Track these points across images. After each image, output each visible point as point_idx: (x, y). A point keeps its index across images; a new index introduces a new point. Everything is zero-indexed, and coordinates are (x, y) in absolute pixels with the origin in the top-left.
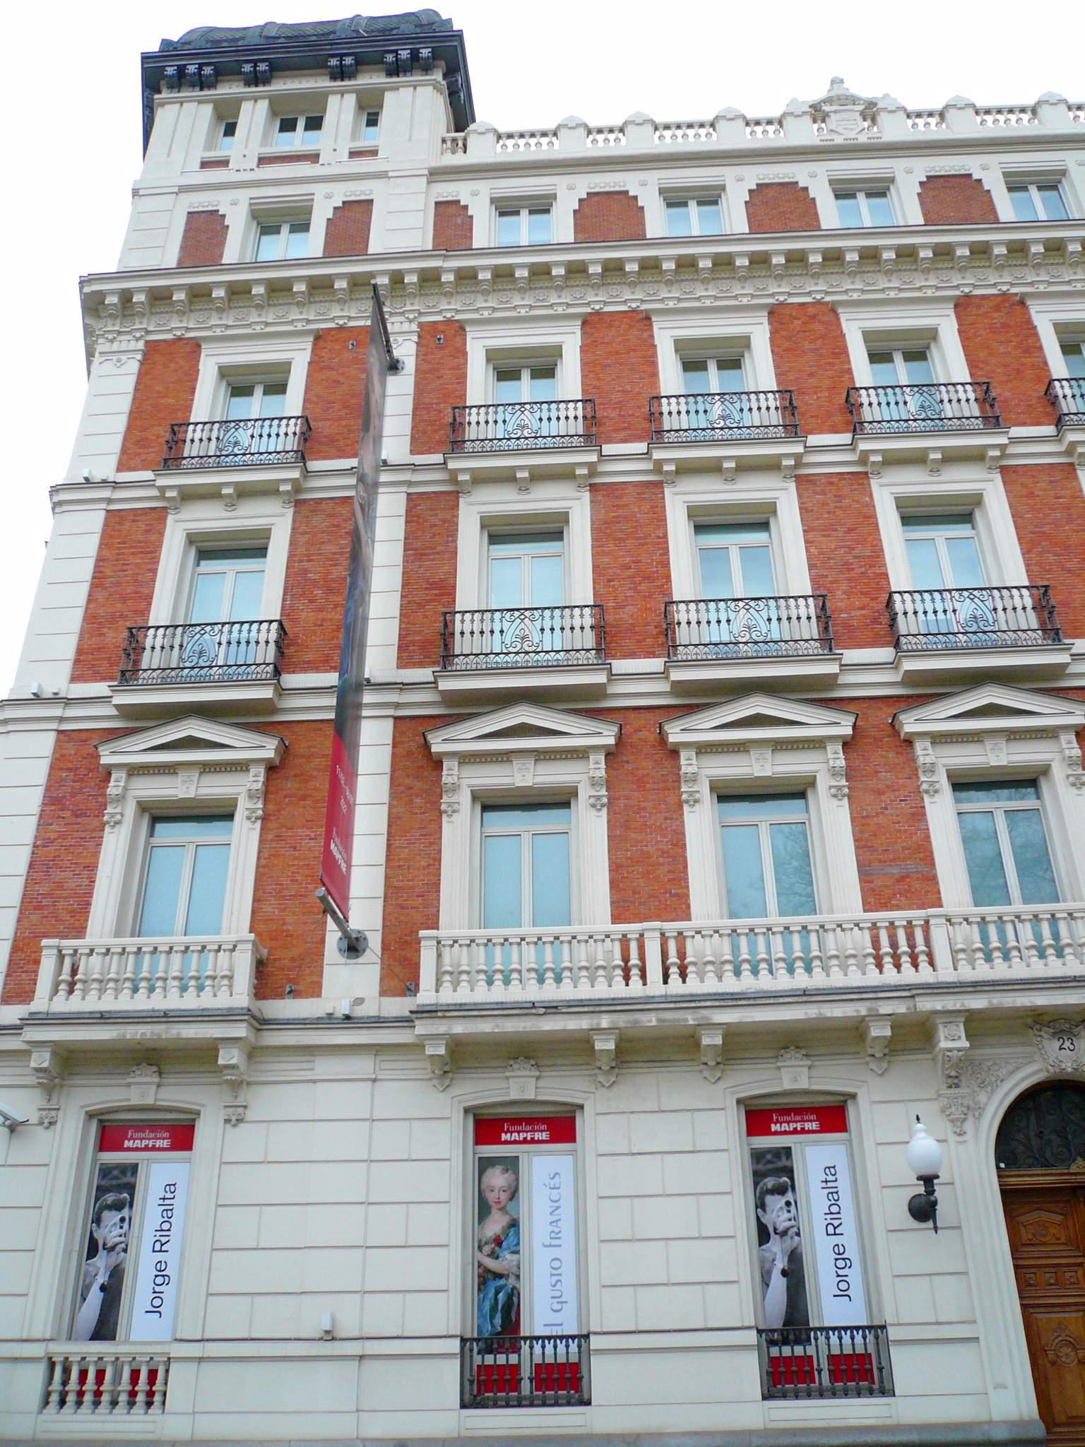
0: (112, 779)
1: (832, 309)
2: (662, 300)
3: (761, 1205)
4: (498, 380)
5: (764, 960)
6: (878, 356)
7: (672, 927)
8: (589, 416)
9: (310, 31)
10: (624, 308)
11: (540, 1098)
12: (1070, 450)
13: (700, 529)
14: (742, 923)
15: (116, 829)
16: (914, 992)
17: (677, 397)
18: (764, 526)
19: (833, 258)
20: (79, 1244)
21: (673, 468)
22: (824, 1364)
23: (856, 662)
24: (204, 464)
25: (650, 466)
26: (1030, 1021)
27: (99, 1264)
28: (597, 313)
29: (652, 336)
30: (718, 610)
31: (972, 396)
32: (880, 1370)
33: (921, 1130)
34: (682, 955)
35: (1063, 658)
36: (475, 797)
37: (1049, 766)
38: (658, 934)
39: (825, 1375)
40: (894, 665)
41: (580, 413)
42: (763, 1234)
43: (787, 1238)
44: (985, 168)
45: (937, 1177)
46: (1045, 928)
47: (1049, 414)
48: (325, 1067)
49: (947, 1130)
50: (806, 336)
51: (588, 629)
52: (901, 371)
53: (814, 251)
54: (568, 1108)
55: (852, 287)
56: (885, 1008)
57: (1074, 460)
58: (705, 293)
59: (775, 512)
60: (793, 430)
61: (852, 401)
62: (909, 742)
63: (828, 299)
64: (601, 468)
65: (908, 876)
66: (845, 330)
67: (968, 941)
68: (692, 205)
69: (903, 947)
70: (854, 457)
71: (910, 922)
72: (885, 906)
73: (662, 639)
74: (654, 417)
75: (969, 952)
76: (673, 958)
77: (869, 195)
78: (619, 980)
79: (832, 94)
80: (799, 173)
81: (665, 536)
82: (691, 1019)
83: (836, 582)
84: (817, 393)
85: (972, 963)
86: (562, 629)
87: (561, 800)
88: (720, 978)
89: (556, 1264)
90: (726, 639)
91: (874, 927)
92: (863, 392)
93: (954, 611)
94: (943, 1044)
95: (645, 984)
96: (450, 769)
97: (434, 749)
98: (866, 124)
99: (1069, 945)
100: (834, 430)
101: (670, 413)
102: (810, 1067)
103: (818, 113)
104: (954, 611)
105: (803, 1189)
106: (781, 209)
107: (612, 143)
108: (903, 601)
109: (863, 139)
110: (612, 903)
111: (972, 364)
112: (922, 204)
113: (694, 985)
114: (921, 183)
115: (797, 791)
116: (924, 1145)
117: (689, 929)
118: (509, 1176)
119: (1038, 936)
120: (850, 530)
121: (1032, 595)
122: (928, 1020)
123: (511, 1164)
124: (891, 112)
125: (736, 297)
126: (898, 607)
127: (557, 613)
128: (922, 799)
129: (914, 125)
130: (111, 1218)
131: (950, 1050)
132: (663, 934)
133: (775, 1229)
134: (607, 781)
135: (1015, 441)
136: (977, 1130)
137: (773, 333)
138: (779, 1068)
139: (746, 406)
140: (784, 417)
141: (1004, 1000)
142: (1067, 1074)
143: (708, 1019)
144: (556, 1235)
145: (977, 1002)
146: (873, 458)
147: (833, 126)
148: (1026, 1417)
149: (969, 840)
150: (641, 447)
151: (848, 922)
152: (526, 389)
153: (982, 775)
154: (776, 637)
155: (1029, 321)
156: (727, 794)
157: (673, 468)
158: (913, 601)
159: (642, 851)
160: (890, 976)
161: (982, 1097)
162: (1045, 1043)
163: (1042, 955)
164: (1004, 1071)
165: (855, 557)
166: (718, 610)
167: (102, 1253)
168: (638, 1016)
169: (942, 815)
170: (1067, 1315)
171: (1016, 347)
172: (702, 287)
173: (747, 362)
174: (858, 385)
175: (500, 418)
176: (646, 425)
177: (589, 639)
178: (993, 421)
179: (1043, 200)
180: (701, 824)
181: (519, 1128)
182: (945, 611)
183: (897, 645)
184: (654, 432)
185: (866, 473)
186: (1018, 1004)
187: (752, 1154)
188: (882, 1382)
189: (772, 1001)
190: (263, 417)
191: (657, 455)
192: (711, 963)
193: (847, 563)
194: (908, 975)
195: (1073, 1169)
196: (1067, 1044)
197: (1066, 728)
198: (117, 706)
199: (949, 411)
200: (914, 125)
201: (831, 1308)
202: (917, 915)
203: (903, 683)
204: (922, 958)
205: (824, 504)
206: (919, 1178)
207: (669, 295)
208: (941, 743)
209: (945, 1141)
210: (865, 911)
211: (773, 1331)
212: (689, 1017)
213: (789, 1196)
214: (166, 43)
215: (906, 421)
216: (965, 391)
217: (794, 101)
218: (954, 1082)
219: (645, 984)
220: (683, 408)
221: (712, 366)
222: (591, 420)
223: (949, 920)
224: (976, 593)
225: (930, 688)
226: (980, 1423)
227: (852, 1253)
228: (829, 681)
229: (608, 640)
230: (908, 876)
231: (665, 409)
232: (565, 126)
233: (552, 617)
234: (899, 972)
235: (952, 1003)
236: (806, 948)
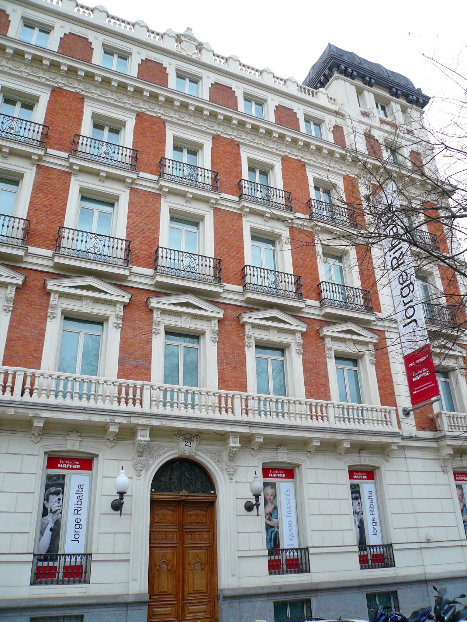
1: (164, 122)
2: (92, 93)
3: (47, 499)
4: (4, 102)
5: (69, 392)
6: (177, 148)
7: (30, 371)
8: (44, 133)
9: (365, 66)
10: (73, 90)
11: (81, 450)
12: (241, 209)
13: (83, 198)
14: (63, 374)
15: (54, 320)
16: (131, 415)
17: (87, 138)
18: (112, 205)
19: (169, 101)
21: (105, 175)
22: (284, 562)
23: (140, 273)
25: (67, 164)
26: (176, 433)
27: (49, 519)
28: (60, 88)
29: (83, 107)
30: (83, 236)
31: (210, 176)
32: (86, 572)
33: (123, 473)
34: (32, 384)
35: (220, 290)
36: (63, 313)
38: (23, 373)
39: (61, 575)
40: (153, 277)
41: (40, 131)
42: (45, 512)
43: (56, 515)
44: (238, 88)
45: (126, 493)
46: (190, 396)
47: (237, 192)
48: (409, 453)
49: (133, 473)
50: (150, 130)
51: (20, 230)
52: (185, 157)
53: (192, 105)
54: (90, 456)
55: (173, 116)
56: (118, 420)
57: (243, 213)
58: (112, 97)
59: (118, 200)
60: (134, 167)
61: (162, 163)
62: (151, 310)
63: (163, 117)
65: (139, 366)
66: (166, 133)
67: (158, 397)
68: (116, 56)
69: (131, 396)
70: (157, 187)
71: (135, 386)
72: (127, 377)
73: (54, 242)
74: (75, 143)
75: (112, 397)
76: (28, 385)
77: (190, 81)
78: (116, 403)
79: (186, 33)
80: (91, 35)
81: (67, 197)
82: (30, 413)
83: (137, 237)
84: (147, 155)
85: (158, 406)
86: (8, 226)
87: (99, 322)
88: (48, 397)
89: (290, 523)
90: (83, 249)
91: (166, 390)
92: (167, 161)
93: (182, 261)
94: (139, 438)
95: (12, 395)
97: (49, 287)
98: (197, 51)
99: (197, 405)
100: (152, 173)
101: (82, 144)
102: (81, 441)
103: (178, 38)
104: (182, 261)
105: (67, 494)
106: (154, 73)
107: (86, 15)
108: (163, 252)
109: (194, 57)
110: (5, 356)
111: (213, 163)
112: (210, 92)
113: (35, 399)
114: (212, 84)
115: (100, 321)
116: (123, 479)
117: (38, 373)
118: (273, 490)
119: (186, 400)
120: (148, 216)
121: (214, 262)
122: (251, 436)
123: (273, 485)
124: (100, 11)
125: (124, 103)
126: (160, 253)
127: (7, 218)
128: (152, 335)
129: (241, 69)
130: (53, 499)
131: (141, 441)
132: (25, 374)
133: (51, 510)
134: (14, 300)
135: (222, 199)
136: (146, 475)
137: (136, 124)
138: (67, 440)
139: (117, 151)
140: (132, 161)
141: (167, 423)
142: (186, 456)
143: (38, 414)
144: (289, 512)
145: (156, 423)
146: (165, 189)
147: (182, 47)
148: (142, 592)
149: (167, 356)
150: (65, 155)
151: (110, 381)
152: (17, 111)
153: (95, 318)
154: (106, 253)
155: (239, 153)
156: (68, 317)
157: (167, 190)
158: (167, 253)
159: (24, 335)
160: (123, 407)
161: (151, 462)
162: (180, 442)
163: (186, 407)
164: (162, 452)
165: (147, 228)
166: (83, 236)
168: (5, 409)
169: (159, 343)
170: (167, 551)
171: (232, 162)
172: (111, 94)
173: (122, 132)
175: (97, 146)
176: (70, 145)
177: (20, 234)
178: (216, 188)
179: (118, 62)
180: (54, 328)
181: (67, 462)
182: (178, 260)
183: (156, 269)
184: (73, 150)
185: (160, 195)
186: (173, 426)
187: (47, 477)
188: (85, 577)
189: (69, 410)
191: (72, 160)
192: (45, 390)
193: (143, 230)
194: (130, 408)
195: (181, 494)
196: (188, 444)
197: (215, 318)
199: (200, 179)
200: (241, 69)
201: (69, 545)
202: (139, 383)
203: (323, 316)
204: (138, 401)
205: (140, 203)
206: (118, 493)
207: (95, 92)
208: (164, 313)
209: (132, 478)
210: (118, 378)
211: (42, 555)
212: (30, 413)
213: (60, 496)
214: (419, 90)
215: (182, 178)
216: (208, 173)
217: (170, 29)
218: (140, 454)
219: (12, 395)
220: (89, 144)
221: (106, 129)
222: (45, 135)
223: (152, 387)
224: (192, 255)
225: (255, 306)
226: (123, 595)
227: (84, 522)
228: (124, 278)
229: (29, 236)
230: (139, 366)
231: (81, 141)
232: (98, 9)
233: (9, 221)
234: (134, 406)
235: (146, 422)
236: (89, 390)
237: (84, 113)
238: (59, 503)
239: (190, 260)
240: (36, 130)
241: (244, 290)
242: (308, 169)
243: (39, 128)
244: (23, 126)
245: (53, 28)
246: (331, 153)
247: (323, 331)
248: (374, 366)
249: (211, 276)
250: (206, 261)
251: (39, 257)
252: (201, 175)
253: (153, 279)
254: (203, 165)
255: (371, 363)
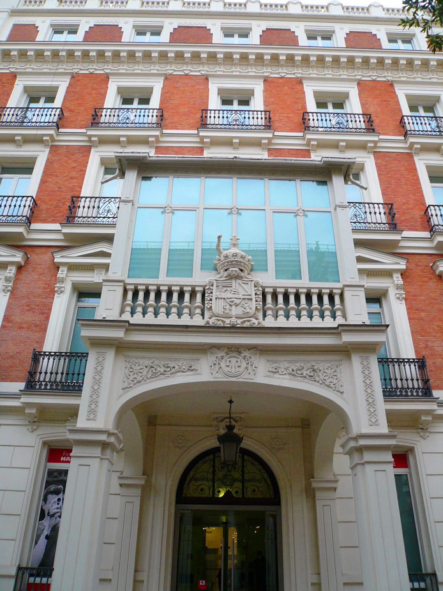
0: (8, 269)
3: (45, 500)
15: (61, 295)
20: (35, 513)
24: (109, 126)
27: (45, 524)
37: (388, 289)
43: (53, 518)
62: (57, 267)
64: (274, 141)
92: (310, 114)
96: (62, 271)
130: (52, 498)
133: (49, 513)
167: (47, 518)
174: (308, 111)
175: (225, 116)
183: (431, 231)
190: (219, 109)
198: (64, 234)
211: (34, 569)
213: (60, 496)
224: (357, 205)
237: (399, 96)
238: (58, 504)
239: (355, 210)
240: (260, 117)
241: (432, 236)
242: (305, 84)
243: (261, 114)
244: (247, 116)
245: (334, 32)
246: (260, 58)
247: (438, 267)
248: (404, 301)
249: (384, 224)
250: (374, 208)
251: (47, 232)
252: (352, 121)
253: (432, 241)
254: (352, 110)
255: (398, 298)
